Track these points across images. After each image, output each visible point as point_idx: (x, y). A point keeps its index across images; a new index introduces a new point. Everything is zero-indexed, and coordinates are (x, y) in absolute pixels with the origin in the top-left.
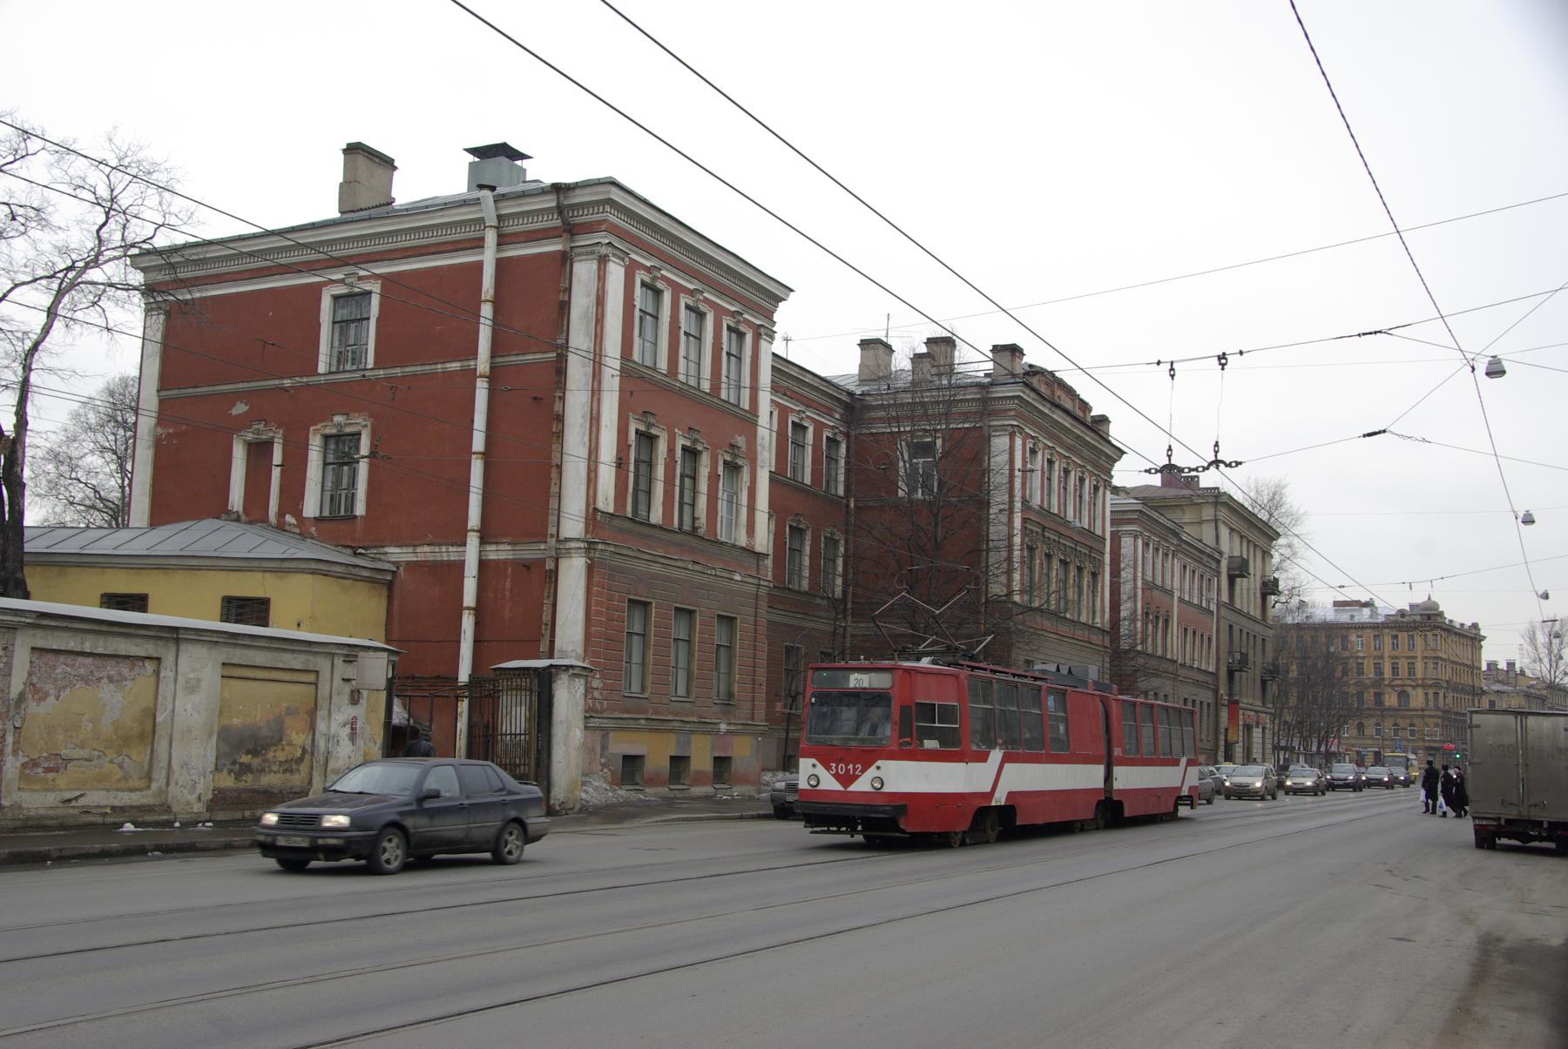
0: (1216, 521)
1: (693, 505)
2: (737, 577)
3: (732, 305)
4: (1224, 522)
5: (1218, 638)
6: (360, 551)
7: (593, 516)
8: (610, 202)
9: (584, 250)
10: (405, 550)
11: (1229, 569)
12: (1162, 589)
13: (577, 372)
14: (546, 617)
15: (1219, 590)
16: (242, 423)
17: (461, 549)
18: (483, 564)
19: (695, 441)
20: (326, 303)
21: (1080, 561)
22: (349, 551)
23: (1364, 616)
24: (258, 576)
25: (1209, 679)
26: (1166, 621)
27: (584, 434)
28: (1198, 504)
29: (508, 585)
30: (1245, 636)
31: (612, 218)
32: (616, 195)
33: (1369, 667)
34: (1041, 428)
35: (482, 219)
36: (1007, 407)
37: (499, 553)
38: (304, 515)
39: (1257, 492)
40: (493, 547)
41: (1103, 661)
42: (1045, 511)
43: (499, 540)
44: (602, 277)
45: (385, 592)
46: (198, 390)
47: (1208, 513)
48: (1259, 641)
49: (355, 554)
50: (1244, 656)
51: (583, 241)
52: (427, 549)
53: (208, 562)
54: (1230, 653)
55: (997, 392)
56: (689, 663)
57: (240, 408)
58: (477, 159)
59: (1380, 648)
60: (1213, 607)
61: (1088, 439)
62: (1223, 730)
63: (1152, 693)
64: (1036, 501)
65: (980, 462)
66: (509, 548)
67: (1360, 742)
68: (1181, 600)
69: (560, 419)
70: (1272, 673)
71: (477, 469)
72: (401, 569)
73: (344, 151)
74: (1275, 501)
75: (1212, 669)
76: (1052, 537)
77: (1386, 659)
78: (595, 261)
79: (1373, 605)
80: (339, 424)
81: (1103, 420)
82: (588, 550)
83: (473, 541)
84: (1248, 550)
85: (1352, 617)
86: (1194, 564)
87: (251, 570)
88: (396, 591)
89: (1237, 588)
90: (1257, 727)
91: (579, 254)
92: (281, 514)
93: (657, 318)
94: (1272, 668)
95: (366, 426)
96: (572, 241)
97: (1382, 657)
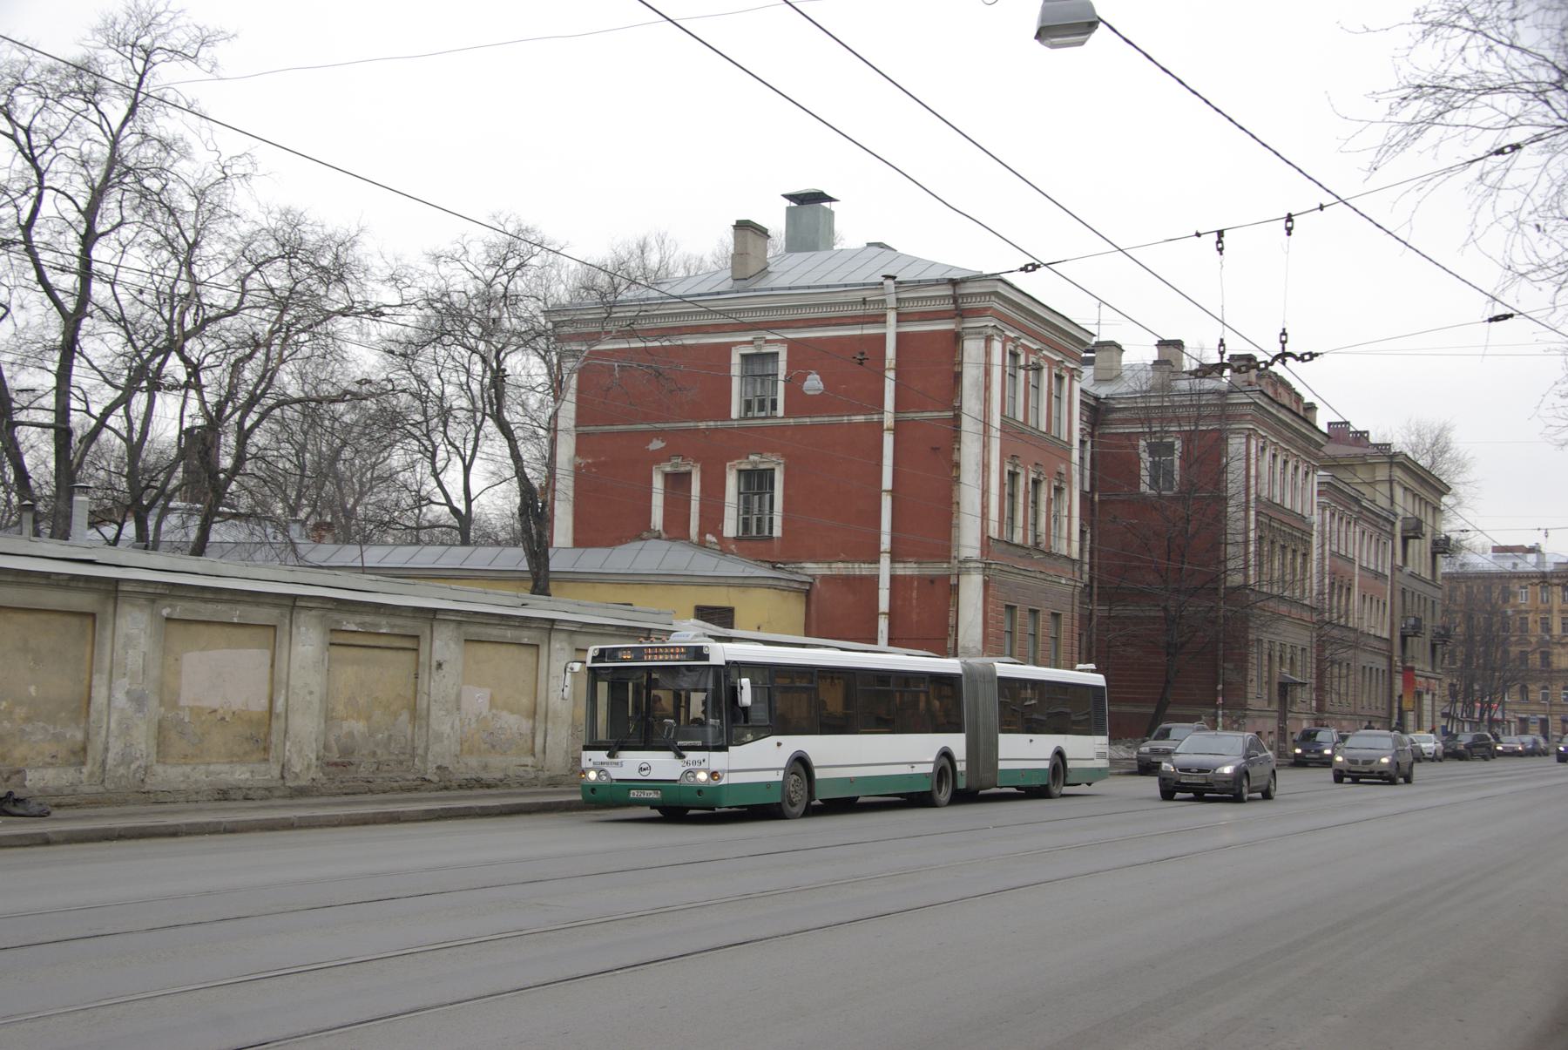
0: (1391, 481)
1: (1035, 525)
2: (1063, 581)
3: (1057, 355)
4: (1399, 482)
5: (1392, 604)
6: (779, 565)
7: (986, 541)
8: (997, 294)
9: (971, 330)
10: (821, 565)
11: (1403, 530)
12: (1345, 558)
13: (969, 426)
14: (952, 621)
15: (1393, 554)
16: (659, 457)
17: (877, 566)
18: (893, 578)
19: (1038, 476)
20: (736, 359)
21: (1284, 540)
22: (767, 565)
23: (1529, 563)
24: (724, 590)
25: (1383, 646)
26: (1349, 589)
27: (978, 479)
28: (1371, 464)
29: (914, 594)
30: (1416, 599)
31: (996, 306)
32: (1002, 289)
33: (1535, 630)
34: (1270, 428)
35: (884, 301)
36: (1243, 412)
37: (908, 569)
38: (725, 535)
39: (1419, 435)
40: (901, 565)
41: (1311, 637)
42: (1270, 503)
43: (905, 559)
44: (988, 353)
45: (804, 599)
46: (615, 427)
47: (1382, 473)
48: (1429, 603)
49: (774, 568)
50: (1418, 620)
51: (971, 323)
52: (841, 565)
53: (682, 579)
54: (1404, 617)
55: (1233, 399)
56: (1035, 652)
57: (656, 445)
58: (793, 204)
59: (1548, 601)
60: (1388, 572)
61: (1303, 430)
62: (1397, 698)
63: (1345, 664)
64: (1265, 494)
65: (1219, 460)
66: (915, 566)
67: (1524, 707)
68: (1360, 566)
69: (957, 465)
70: (1442, 637)
71: (886, 503)
72: (817, 581)
73: (734, 227)
74: (1439, 446)
75: (1386, 635)
76: (1276, 525)
77: (1555, 613)
78: (983, 341)
79: (1539, 551)
80: (754, 462)
81: (1311, 407)
82: (984, 569)
83: (885, 561)
84: (1420, 509)
85: (1515, 565)
86: (1372, 529)
87: (718, 585)
88: (813, 597)
89: (1410, 550)
90: (1427, 693)
91: (969, 334)
92: (702, 533)
93: (1037, 388)
94: (1443, 632)
95: (779, 464)
96: (963, 323)
97: (1550, 611)
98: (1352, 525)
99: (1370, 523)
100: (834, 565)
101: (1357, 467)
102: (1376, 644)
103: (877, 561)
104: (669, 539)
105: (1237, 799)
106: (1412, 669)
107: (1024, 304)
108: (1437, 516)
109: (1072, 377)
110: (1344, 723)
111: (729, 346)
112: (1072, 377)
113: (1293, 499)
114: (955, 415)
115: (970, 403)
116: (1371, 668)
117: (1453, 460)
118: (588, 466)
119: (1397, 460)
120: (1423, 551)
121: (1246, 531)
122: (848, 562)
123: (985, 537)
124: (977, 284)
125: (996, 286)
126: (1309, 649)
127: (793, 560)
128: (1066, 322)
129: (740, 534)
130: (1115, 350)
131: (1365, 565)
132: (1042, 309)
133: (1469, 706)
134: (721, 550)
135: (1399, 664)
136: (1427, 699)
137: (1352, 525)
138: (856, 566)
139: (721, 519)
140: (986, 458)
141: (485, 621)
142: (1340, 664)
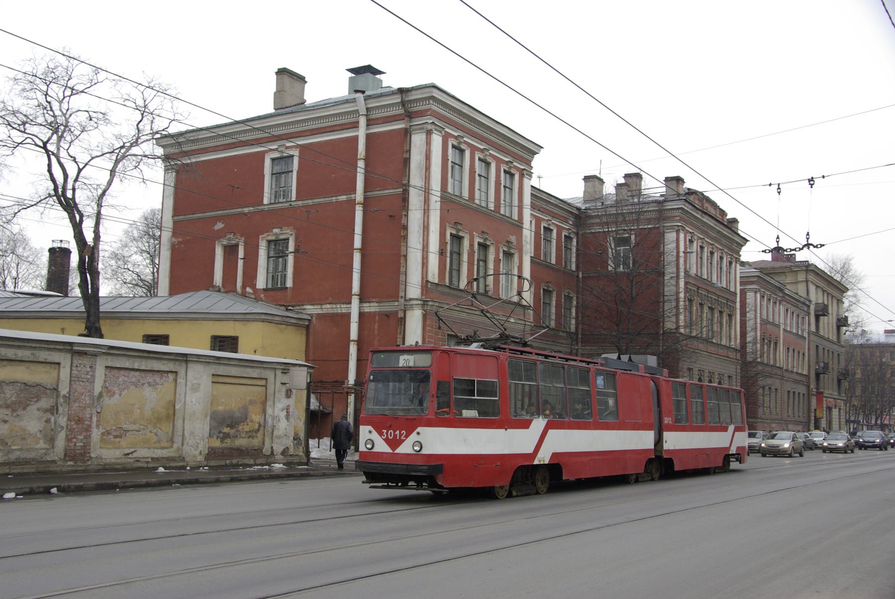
0: (807, 281)
3: (507, 157)
4: (812, 282)
6: (290, 308)
7: (426, 285)
10: (316, 307)
11: (816, 311)
12: (773, 324)
13: (415, 199)
15: (809, 324)
16: (220, 235)
18: (361, 315)
20: (268, 163)
21: (721, 308)
24: (231, 323)
25: (804, 379)
26: (776, 343)
27: (420, 237)
28: (794, 271)
29: (376, 327)
31: (434, 108)
32: (436, 94)
35: (357, 111)
36: (674, 214)
37: (371, 308)
38: (258, 287)
40: (367, 305)
41: (736, 369)
42: (698, 278)
43: (371, 300)
44: (428, 143)
45: (305, 332)
46: (195, 216)
47: (801, 277)
48: (836, 355)
49: (287, 310)
52: (328, 306)
54: (817, 363)
55: (668, 205)
57: (219, 226)
58: (353, 75)
61: (725, 233)
62: (813, 410)
63: (767, 388)
64: (693, 271)
66: (376, 305)
68: (785, 330)
69: (405, 228)
70: (844, 376)
71: (357, 258)
72: (314, 318)
74: (845, 268)
75: (805, 372)
78: (425, 134)
80: (276, 234)
82: (423, 305)
83: (355, 301)
84: (828, 300)
86: (793, 309)
88: (311, 331)
89: (821, 322)
90: (835, 408)
92: (244, 287)
95: (292, 235)
98: (778, 304)
99: (792, 305)
100: (324, 306)
101: (787, 274)
102: (798, 378)
103: (350, 303)
104: (226, 292)
105: (846, 452)
106: (822, 393)
107: (465, 111)
108: (840, 304)
109: (522, 176)
110: (773, 425)
111: (261, 155)
112: (522, 176)
113: (720, 278)
114: (404, 190)
115: (416, 179)
116: (794, 392)
117: (854, 276)
118: (179, 243)
119: (811, 268)
120: (830, 325)
121: (678, 293)
122: (333, 304)
123: (424, 282)
124: (419, 92)
125: (432, 92)
126: (734, 377)
127: (299, 304)
128: (510, 132)
129: (270, 286)
130: (597, 182)
131: (789, 329)
132: (501, 127)
133: (867, 416)
134: (255, 299)
135: (815, 390)
136: (835, 412)
137: (778, 304)
138: (338, 306)
139: (255, 277)
140: (426, 221)
141: (247, 364)
142: (764, 388)
